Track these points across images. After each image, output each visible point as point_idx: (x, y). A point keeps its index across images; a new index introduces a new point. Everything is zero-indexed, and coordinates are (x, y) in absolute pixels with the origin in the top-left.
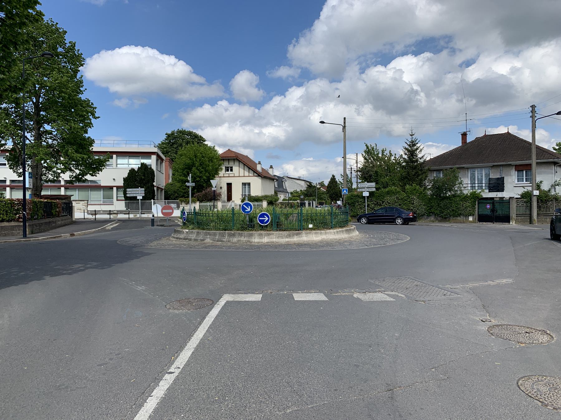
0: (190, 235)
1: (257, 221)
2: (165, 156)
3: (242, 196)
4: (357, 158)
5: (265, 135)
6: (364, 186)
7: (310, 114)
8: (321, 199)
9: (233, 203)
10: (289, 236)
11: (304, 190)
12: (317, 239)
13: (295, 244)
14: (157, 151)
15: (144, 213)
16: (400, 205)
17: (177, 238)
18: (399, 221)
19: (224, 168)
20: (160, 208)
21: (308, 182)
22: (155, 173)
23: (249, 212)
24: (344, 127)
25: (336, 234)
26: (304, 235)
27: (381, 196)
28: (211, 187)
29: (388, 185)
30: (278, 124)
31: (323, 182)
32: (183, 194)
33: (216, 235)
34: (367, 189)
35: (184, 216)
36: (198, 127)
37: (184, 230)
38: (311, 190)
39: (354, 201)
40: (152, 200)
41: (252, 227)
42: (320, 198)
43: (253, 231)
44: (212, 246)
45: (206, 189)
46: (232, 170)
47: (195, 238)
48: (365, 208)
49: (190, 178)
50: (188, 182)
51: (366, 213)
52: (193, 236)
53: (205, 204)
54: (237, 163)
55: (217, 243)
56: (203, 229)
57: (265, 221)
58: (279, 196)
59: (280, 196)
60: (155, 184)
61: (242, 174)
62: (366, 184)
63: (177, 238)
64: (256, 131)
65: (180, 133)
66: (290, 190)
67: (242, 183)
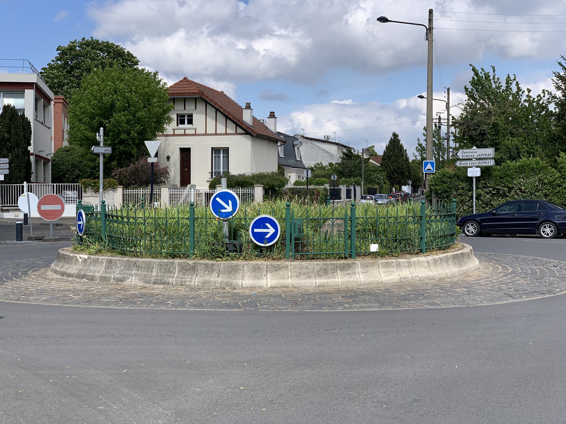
0: (92, 268)
1: (249, 235)
2: (56, 93)
3: (212, 175)
4: (448, 99)
5: (258, 53)
6: (471, 154)
7: (347, 12)
8: (371, 181)
9: (192, 189)
10: (325, 272)
11: (336, 163)
12: (388, 278)
13: (339, 291)
14: (36, 81)
15: (8, 211)
16: (546, 195)
17: (62, 274)
18: (548, 230)
19: (174, 117)
20: (34, 199)
21: (345, 147)
22: (32, 127)
23: (230, 214)
24: (430, 30)
25: (433, 268)
26: (359, 269)
27: (505, 177)
28: (147, 156)
29: (520, 152)
30: (283, 32)
31: (373, 147)
32: (90, 170)
33: (153, 268)
34: (477, 162)
35: (79, 223)
36: (126, 37)
37: (78, 256)
38: (350, 163)
39: (449, 187)
40: (25, 182)
41: (236, 251)
42: (369, 181)
43: (239, 259)
44: (143, 295)
45: (137, 160)
46: (190, 122)
47: (104, 275)
48: (472, 202)
49: (102, 137)
50: (97, 144)
51: (474, 213)
52: (99, 270)
53: (134, 191)
54: (201, 107)
55: (153, 289)
56: (123, 253)
57: (268, 236)
58: (287, 175)
59: (289, 174)
60: (31, 149)
61: (211, 130)
62: (475, 152)
63: (62, 274)
64: (241, 46)
65: (88, 46)
66: (309, 163)
67: (212, 148)
